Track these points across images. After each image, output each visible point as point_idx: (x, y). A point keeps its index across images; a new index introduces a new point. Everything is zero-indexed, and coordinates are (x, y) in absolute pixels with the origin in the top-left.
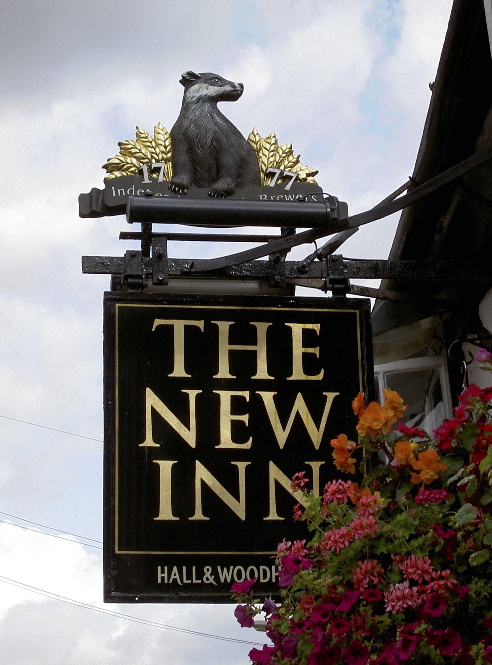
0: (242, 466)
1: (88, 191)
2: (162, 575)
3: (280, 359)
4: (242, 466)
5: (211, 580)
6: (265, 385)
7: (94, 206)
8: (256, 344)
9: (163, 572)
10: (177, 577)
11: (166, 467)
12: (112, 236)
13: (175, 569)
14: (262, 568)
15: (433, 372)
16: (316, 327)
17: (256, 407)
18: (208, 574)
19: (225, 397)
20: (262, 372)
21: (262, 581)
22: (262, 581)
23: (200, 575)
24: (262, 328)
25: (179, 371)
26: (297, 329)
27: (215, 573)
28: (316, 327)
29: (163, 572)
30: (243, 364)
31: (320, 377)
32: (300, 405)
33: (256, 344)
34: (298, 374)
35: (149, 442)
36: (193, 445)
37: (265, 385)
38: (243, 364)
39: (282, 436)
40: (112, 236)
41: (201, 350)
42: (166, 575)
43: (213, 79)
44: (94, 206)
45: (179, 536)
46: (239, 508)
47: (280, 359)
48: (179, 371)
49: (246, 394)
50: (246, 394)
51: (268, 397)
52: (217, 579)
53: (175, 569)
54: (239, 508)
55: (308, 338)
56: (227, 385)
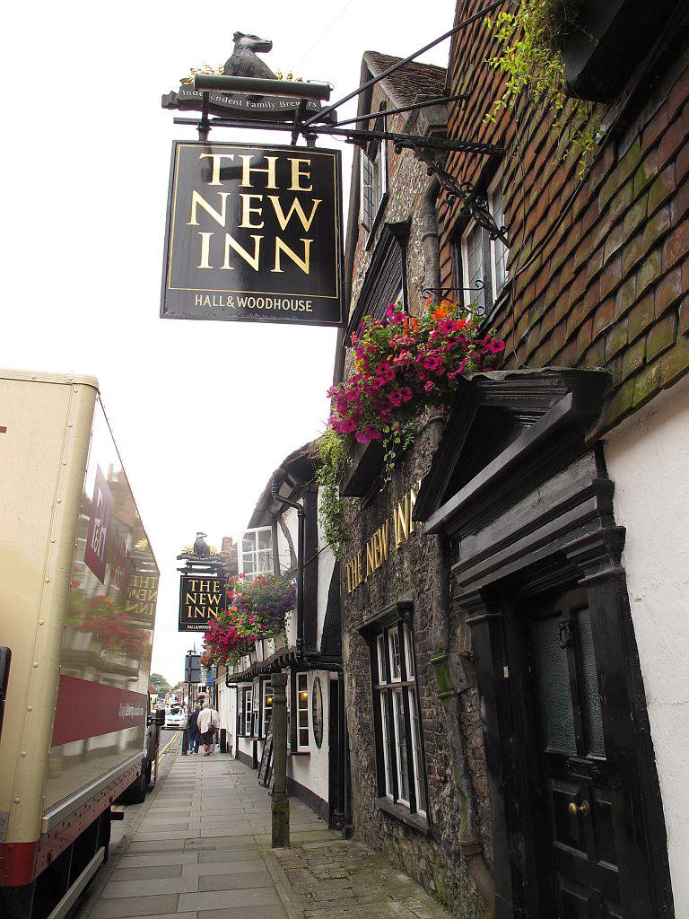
0: (257, 239)
1: (168, 93)
2: (198, 300)
3: (211, 588)
4: (257, 239)
5: (232, 305)
6: (273, 192)
7: (179, 558)
8: (267, 169)
9: (199, 298)
10: (209, 302)
11: (206, 237)
12: (180, 573)
13: (208, 298)
14: (267, 299)
15: (269, 531)
16: (309, 161)
17: (267, 205)
18: (230, 301)
19: (201, 595)
20: (272, 184)
21: (267, 307)
22: (267, 307)
23: (225, 301)
24: (209, 582)
25: (193, 590)
26: (295, 162)
27: (234, 301)
28: (309, 161)
29: (199, 298)
30: (205, 588)
31: (310, 190)
32: (215, 597)
33: (267, 169)
34: (295, 186)
35: (194, 222)
36: (223, 225)
37: (273, 192)
38: (205, 588)
39: (211, 602)
40: (183, 564)
41: (197, 586)
42: (201, 301)
43: (202, 534)
44: (179, 558)
45: (193, 620)
46: (203, 615)
47: (211, 588)
48: (193, 590)
49: (261, 197)
50: (261, 197)
51: (275, 200)
52: (236, 304)
53: (208, 298)
54: (203, 615)
55: (302, 167)
56: (247, 190)
